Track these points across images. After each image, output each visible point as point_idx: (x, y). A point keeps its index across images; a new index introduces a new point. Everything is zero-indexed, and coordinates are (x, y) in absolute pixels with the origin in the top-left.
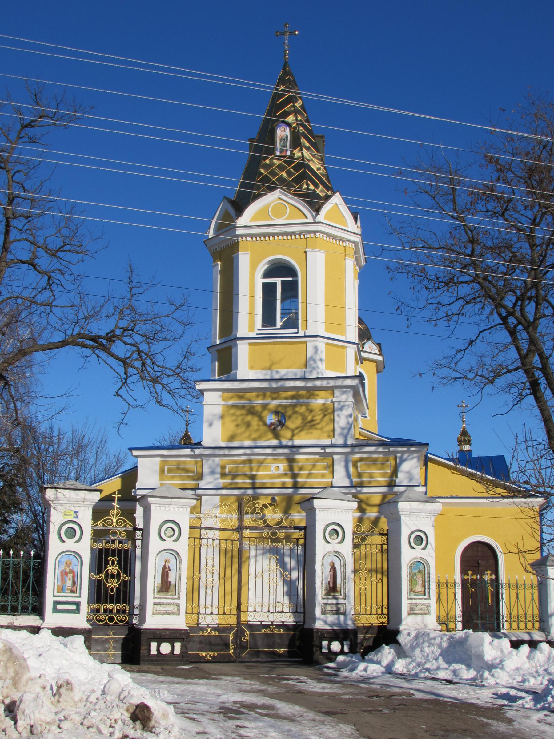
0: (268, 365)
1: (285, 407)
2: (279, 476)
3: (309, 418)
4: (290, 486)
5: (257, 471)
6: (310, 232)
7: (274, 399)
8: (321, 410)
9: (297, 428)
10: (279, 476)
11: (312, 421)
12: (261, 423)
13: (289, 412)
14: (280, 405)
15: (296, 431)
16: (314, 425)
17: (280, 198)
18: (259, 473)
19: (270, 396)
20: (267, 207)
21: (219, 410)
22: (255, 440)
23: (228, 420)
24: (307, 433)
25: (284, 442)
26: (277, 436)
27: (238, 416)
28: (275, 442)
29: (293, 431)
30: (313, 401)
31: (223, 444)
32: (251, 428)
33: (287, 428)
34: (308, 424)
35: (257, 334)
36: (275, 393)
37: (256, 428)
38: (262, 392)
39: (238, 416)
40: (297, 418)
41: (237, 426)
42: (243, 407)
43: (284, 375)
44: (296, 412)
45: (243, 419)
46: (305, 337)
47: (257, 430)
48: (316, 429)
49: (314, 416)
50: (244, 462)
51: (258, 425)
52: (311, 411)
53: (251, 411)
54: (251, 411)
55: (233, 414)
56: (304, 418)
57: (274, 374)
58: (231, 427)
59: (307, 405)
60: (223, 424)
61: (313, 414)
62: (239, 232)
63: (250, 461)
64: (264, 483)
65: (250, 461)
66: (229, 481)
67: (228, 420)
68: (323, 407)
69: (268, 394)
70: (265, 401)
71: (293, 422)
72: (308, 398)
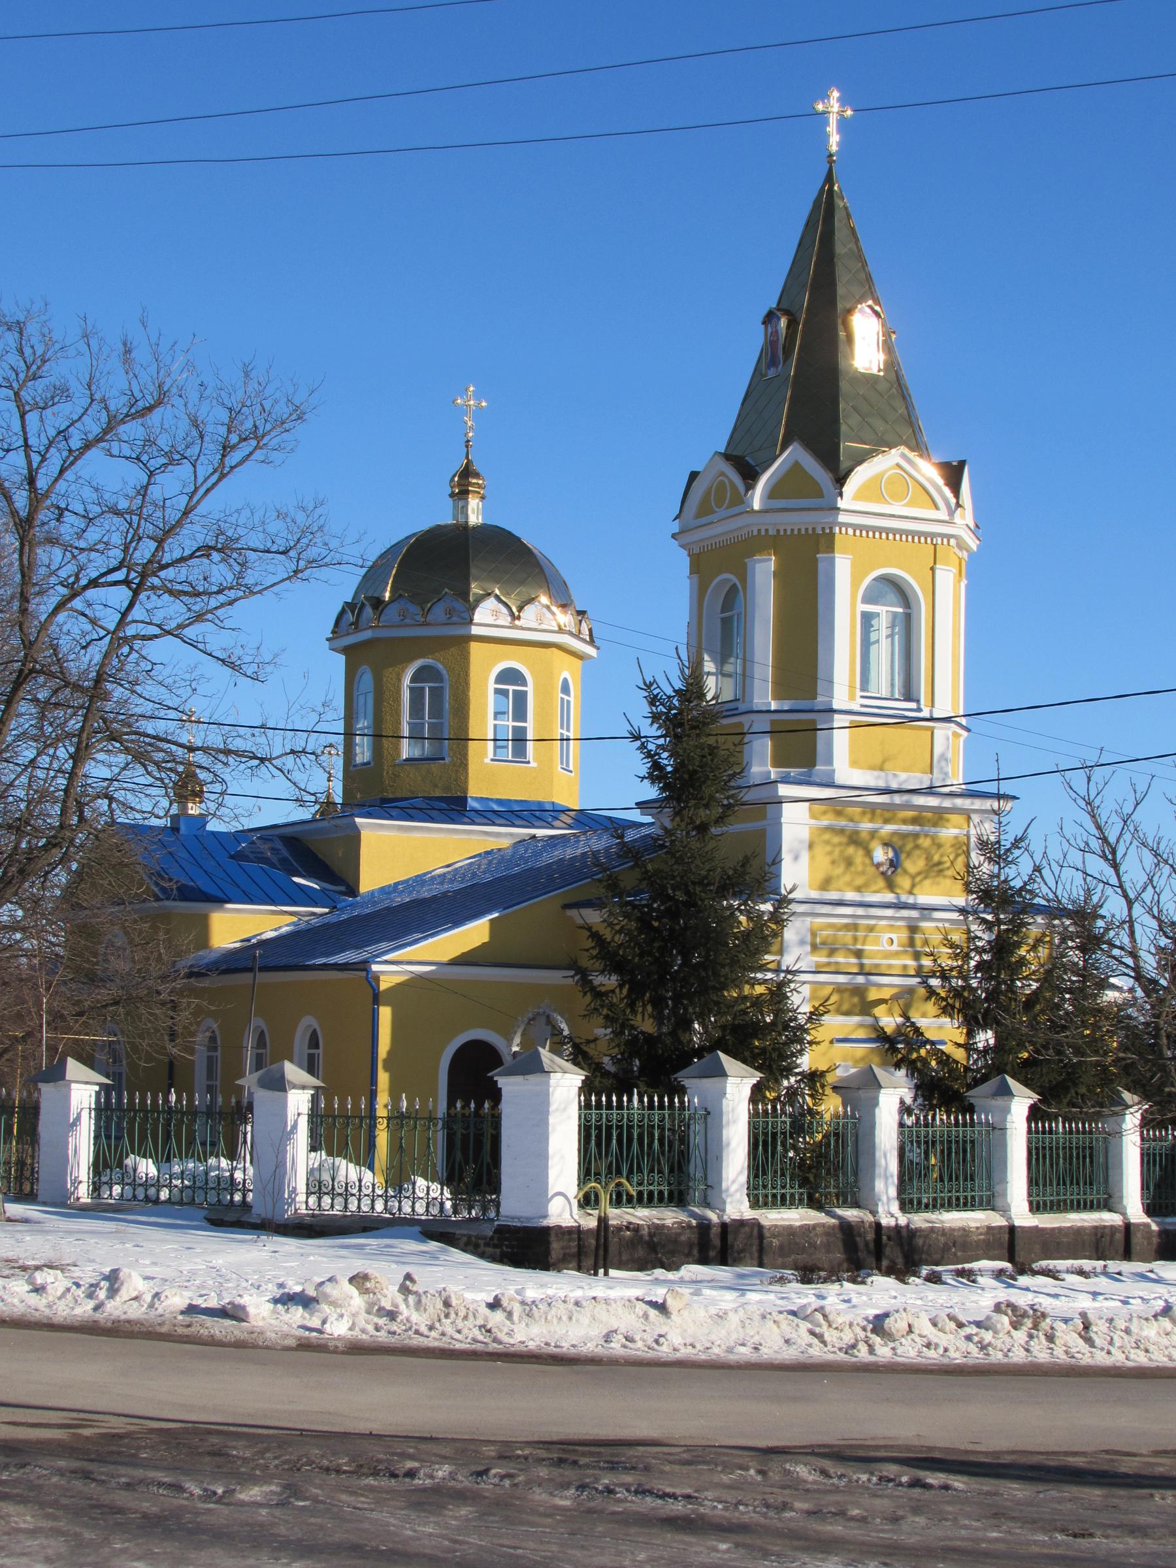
0: (878, 761)
1: (904, 836)
2: (896, 954)
3: (936, 858)
4: (912, 972)
5: (863, 944)
6: (943, 536)
7: (887, 821)
8: (953, 846)
9: (919, 873)
10: (896, 954)
11: (939, 863)
12: (867, 861)
13: (909, 846)
14: (895, 834)
15: (918, 879)
16: (941, 871)
17: (898, 465)
18: (866, 947)
19: (881, 815)
20: (878, 478)
21: (805, 834)
22: (859, 889)
23: (820, 850)
24: (933, 883)
25: (905, 898)
26: (891, 886)
27: (834, 846)
28: (889, 897)
29: (913, 877)
30: (944, 830)
31: (815, 894)
32: (853, 869)
33: (905, 872)
34: (936, 869)
35: (862, 706)
36: (888, 813)
37: (860, 868)
38: (872, 810)
39: (834, 846)
40: (919, 857)
41: (833, 862)
42: (842, 831)
43: (905, 781)
44: (917, 847)
45: (842, 852)
46: (931, 719)
47: (863, 873)
48: (945, 877)
49: (942, 856)
50: (846, 927)
51: (864, 864)
52: (939, 846)
53: (854, 839)
54: (854, 839)
55: (827, 842)
56: (929, 858)
57: (890, 777)
58: (824, 862)
59: (934, 838)
60: (812, 858)
61: (942, 850)
62: (842, 518)
63: (855, 927)
64: (877, 966)
65: (855, 927)
66: (824, 960)
67: (820, 850)
68: (954, 842)
69: (878, 812)
70: (876, 826)
71: (914, 863)
72: (935, 825)
